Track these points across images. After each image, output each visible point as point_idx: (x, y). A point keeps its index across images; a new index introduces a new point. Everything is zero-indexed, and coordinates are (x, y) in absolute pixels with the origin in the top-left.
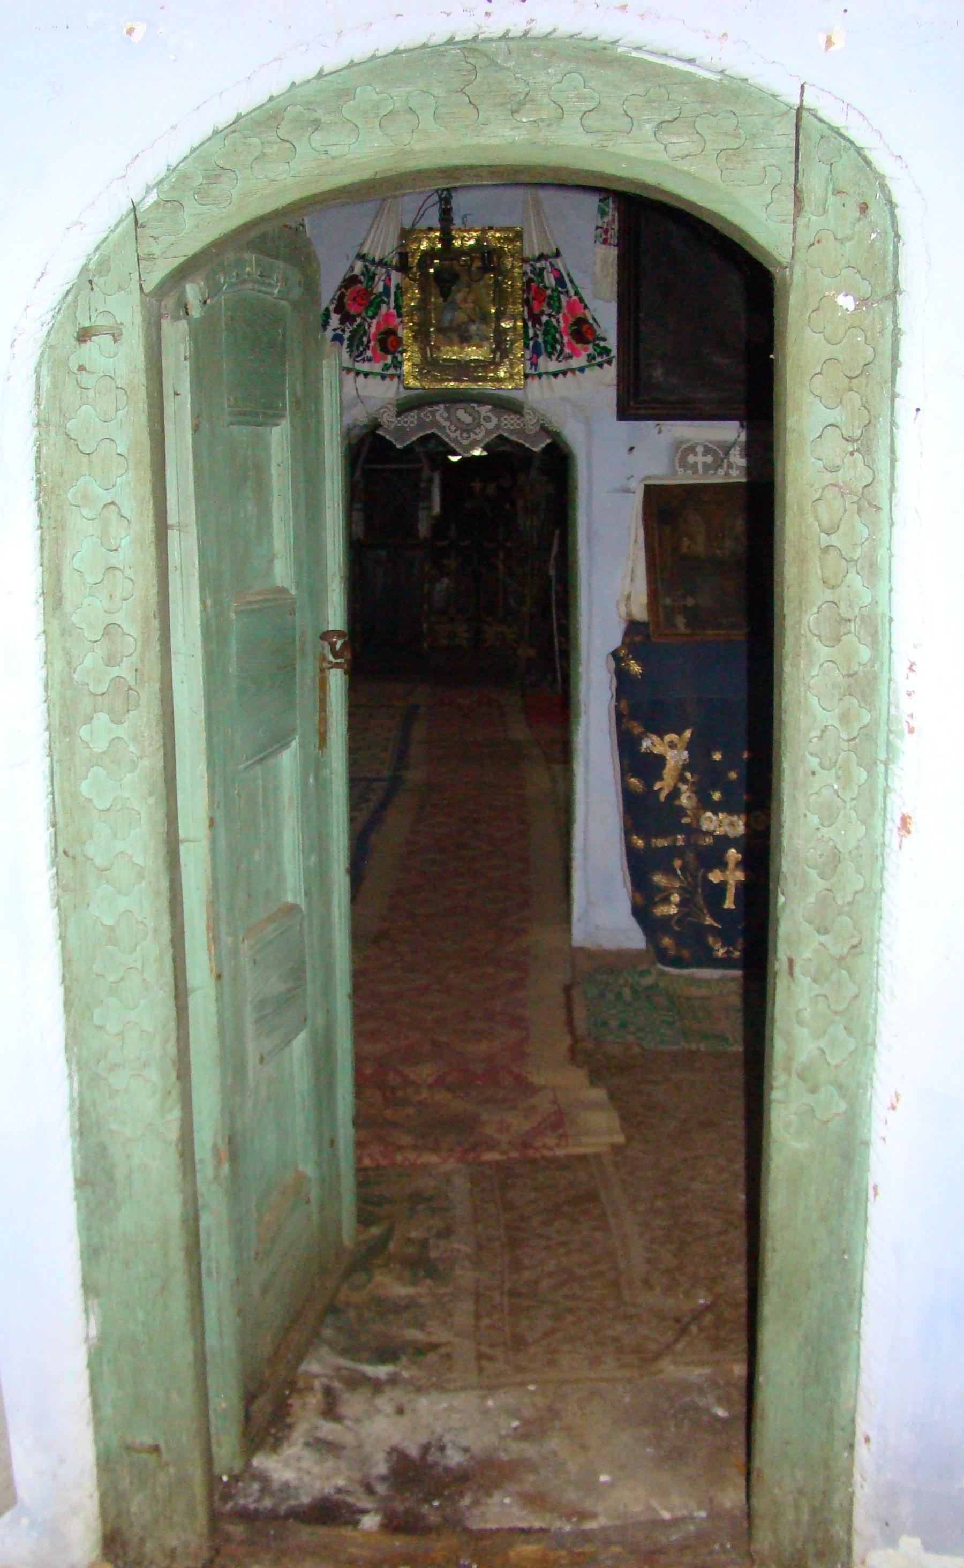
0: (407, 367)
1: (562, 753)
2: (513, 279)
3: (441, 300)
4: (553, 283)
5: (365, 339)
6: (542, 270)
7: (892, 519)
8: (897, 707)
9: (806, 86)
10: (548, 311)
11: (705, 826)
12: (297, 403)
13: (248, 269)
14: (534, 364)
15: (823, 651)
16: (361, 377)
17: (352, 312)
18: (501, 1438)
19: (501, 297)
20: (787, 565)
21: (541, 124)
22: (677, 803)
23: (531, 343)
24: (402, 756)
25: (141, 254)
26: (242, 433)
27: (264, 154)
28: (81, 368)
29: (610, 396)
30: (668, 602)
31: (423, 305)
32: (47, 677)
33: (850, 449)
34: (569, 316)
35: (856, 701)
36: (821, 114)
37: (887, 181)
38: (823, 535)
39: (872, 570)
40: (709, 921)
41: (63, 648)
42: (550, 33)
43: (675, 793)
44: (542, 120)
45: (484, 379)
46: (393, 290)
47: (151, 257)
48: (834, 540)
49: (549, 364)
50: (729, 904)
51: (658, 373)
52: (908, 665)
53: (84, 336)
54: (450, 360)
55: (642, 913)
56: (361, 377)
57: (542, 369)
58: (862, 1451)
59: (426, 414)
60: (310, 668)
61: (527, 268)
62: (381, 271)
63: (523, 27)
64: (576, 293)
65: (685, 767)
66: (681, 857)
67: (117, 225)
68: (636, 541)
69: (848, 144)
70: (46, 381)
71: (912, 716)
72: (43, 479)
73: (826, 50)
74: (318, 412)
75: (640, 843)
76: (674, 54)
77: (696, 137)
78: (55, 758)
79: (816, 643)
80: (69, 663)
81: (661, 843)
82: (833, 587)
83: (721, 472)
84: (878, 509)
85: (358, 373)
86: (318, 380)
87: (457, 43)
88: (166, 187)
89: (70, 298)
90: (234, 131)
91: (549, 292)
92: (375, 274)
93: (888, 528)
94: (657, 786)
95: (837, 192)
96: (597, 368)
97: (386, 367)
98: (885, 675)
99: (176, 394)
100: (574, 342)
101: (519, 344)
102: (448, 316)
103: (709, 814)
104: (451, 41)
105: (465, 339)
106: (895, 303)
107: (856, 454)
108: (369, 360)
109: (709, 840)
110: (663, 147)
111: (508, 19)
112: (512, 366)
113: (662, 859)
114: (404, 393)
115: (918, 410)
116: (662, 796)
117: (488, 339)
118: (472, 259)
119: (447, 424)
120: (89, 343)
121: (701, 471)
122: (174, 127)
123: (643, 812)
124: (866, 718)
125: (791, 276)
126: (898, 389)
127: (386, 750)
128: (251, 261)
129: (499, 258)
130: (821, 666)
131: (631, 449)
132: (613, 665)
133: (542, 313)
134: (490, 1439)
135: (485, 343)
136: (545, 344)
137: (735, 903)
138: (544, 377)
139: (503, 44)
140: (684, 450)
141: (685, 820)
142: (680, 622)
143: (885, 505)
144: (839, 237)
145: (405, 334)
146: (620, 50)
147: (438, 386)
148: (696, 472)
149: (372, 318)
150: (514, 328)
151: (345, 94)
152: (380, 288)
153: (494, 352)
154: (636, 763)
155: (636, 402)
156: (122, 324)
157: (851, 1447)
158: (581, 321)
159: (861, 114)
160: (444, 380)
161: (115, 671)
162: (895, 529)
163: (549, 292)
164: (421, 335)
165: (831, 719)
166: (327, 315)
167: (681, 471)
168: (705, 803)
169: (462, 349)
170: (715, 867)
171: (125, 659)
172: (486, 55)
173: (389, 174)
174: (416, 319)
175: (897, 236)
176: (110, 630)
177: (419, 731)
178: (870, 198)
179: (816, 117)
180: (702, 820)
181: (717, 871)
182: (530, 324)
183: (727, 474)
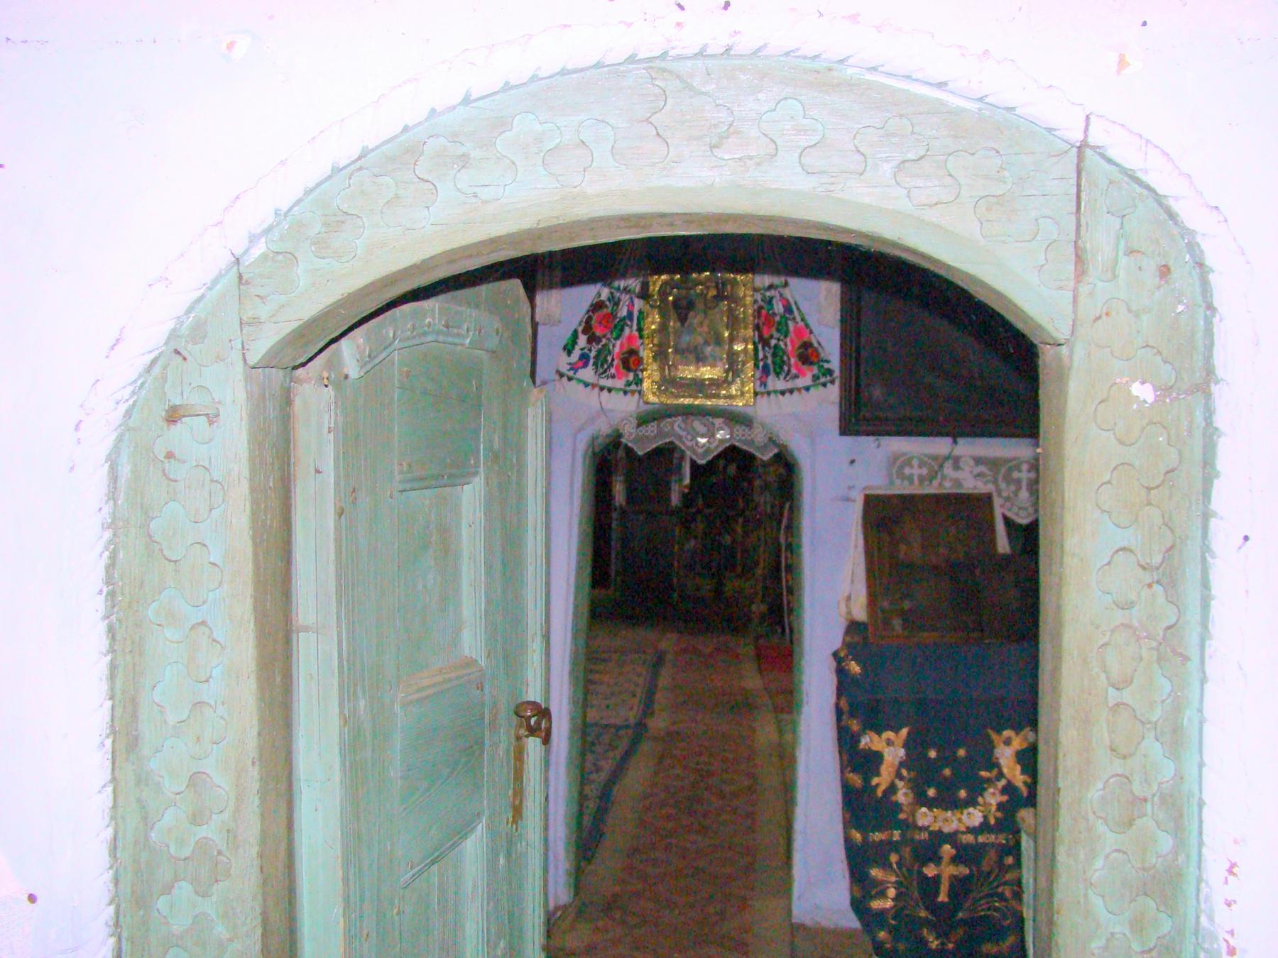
0: (646, 385)
1: (786, 701)
2: (744, 306)
3: (679, 324)
4: (781, 310)
5: (609, 358)
6: (771, 298)
7: (1204, 672)
8: (1211, 919)
9: (1092, 118)
10: (776, 335)
11: (921, 822)
12: (495, 457)
13: (427, 320)
14: (764, 384)
15: (1110, 839)
16: (605, 392)
17: (598, 333)
19: (733, 322)
21: (748, 162)
22: (894, 798)
23: (761, 364)
25: (244, 318)
26: (423, 498)
27: (397, 197)
28: (170, 455)
29: (833, 412)
30: (885, 604)
31: (663, 328)
32: (115, 838)
33: (1149, 581)
34: (796, 340)
35: (1152, 904)
36: (1111, 153)
37: (1199, 239)
38: (1111, 690)
39: (1177, 735)
40: (923, 914)
41: (139, 801)
42: (759, 50)
43: (892, 789)
44: (751, 158)
45: (718, 396)
46: (636, 314)
47: (255, 322)
48: (1126, 696)
49: (775, 383)
50: (943, 897)
51: (877, 392)
52: (1227, 865)
53: (173, 416)
54: (685, 378)
55: (859, 906)
56: (605, 392)
57: (770, 387)
59: (666, 424)
60: (503, 737)
61: (758, 297)
62: (625, 298)
63: (725, 41)
64: (803, 320)
65: (902, 764)
66: (897, 851)
67: (215, 282)
68: (856, 547)
69: (1145, 192)
70: (125, 471)
71: (1232, 933)
72: (118, 591)
73: (1119, 72)
74: (521, 467)
75: (858, 836)
76: (919, 76)
77: (948, 180)
78: (125, 934)
79: (1100, 827)
80: (145, 818)
81: (877, 836)
82: (1125, 757)
83: (935, 483)
84: (1186, 659)
85: (602, 389)
86: (522, 427)
87: (640, 61)
88: (276, 234)
89: (157, 370)
90: (361, 169)
91: (777, 319)
92: (619, 300)
93: (1197, 684)
94: (875, 781)
95: (1131, 252)
96: (821, 388)
97: (629, 384)
98: (1192, 868)
99: (318, 471)
100: (800, 364)
101: (750, 365)
102: (686, 339)
103: (924, 809)
104: (632, 59)
105: (700, 359)
106: (1208, 395)
107: (1155, 586)
108: (613, 377)
109: (924, 836)
110: (905, 192)
111: (705, 30)
112: (743, 384)
113: (878, 854)
114: (643, 408)
115: (1246, 538)
116: (879, 793)
117: (721, 359)
118: (708, 288)
119: (684, 434)
120: (179, 424)
121: (916, 482)
122: (283, 163)
123: (861, 806)
124: (1166, 926)
125: (1071, 356)
126: (1215, 505)
127: (634, 696)
128: (433, 311)
129: (732, 287)
130: (1107, 857)
131: (852, 462)
132: (835, 664)
133: (772, 337)
135: (719, 364)
136: (772, 365)
137: (949, 896)
138: (772, 396)
139: (699, 63)
140: (898, 464)
141: (902, 816)
142: (897, 623)
143: (1194, 653)
144: (1134, 308)
145: (646, 354)
146: (850, 71)
147: (675, 402)
148: (912, 482)
149: (616, 339)
150: (745, 350)
151: (501, 124)
152: (623, 312)
153: (727, 371)
154: (857, 761)
155: (858, 418)
156: (219, 402)
158: (807, 345)
159: (1165, 154)
160: (677, 397)
161: (202, 832)
162: (1208, 687)
163: (777, 319)
164: (660, 355)
165: (1119, 927)
166: (575, 335)
167: (898, 482)
168: (921, 800)
169: (698, 369)
170: (930, 860)
171: (214, 816)
172: (678, 77)
173: (555, 222)
174: (656, 341)
175: (1210, 307)
176: (196, 781)
178: (1176, 261)
179: (1103, 156)
180: (918, 815)
181: (932, 865)
182: (760, 347)
183: (940, 485)
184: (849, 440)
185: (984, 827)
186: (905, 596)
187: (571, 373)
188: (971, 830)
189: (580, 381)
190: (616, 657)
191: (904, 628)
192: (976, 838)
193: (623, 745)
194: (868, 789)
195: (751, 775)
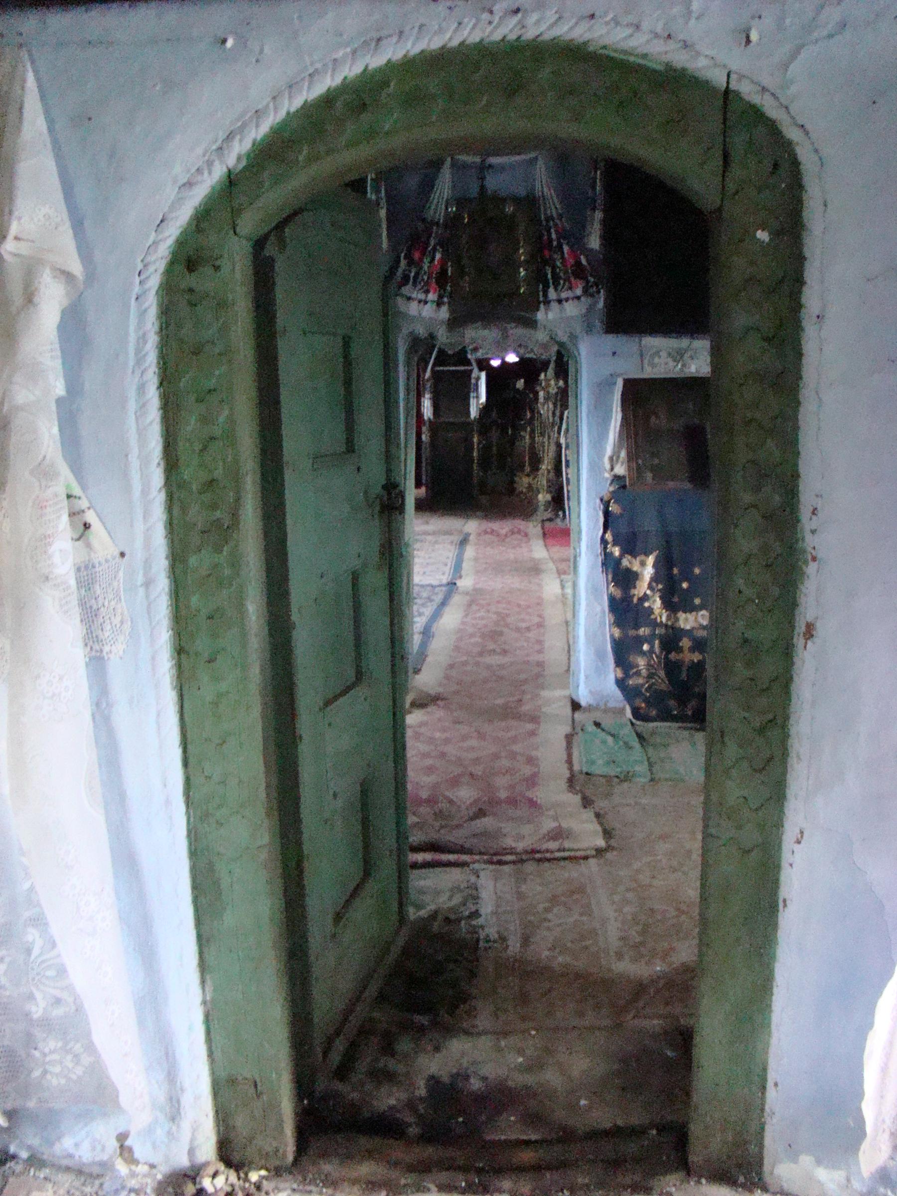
18: (510, 1070)
20: (167, 590)
24: (458, 568)
50: (684, 676)
52: (811, 509)
58: (771, 1094)
71: (814, 548)
116: (635, 600)
127: (446, 565)
131: (614, 353)
134: (502, 1072)
142: (649, 476)
157: (764, 1088)
177: (470, 552)
184: (610, 337)
186: (653, 455)
190: (429, 538)
193: (438, 598)
194: (627, 598)
195: (540, 616)
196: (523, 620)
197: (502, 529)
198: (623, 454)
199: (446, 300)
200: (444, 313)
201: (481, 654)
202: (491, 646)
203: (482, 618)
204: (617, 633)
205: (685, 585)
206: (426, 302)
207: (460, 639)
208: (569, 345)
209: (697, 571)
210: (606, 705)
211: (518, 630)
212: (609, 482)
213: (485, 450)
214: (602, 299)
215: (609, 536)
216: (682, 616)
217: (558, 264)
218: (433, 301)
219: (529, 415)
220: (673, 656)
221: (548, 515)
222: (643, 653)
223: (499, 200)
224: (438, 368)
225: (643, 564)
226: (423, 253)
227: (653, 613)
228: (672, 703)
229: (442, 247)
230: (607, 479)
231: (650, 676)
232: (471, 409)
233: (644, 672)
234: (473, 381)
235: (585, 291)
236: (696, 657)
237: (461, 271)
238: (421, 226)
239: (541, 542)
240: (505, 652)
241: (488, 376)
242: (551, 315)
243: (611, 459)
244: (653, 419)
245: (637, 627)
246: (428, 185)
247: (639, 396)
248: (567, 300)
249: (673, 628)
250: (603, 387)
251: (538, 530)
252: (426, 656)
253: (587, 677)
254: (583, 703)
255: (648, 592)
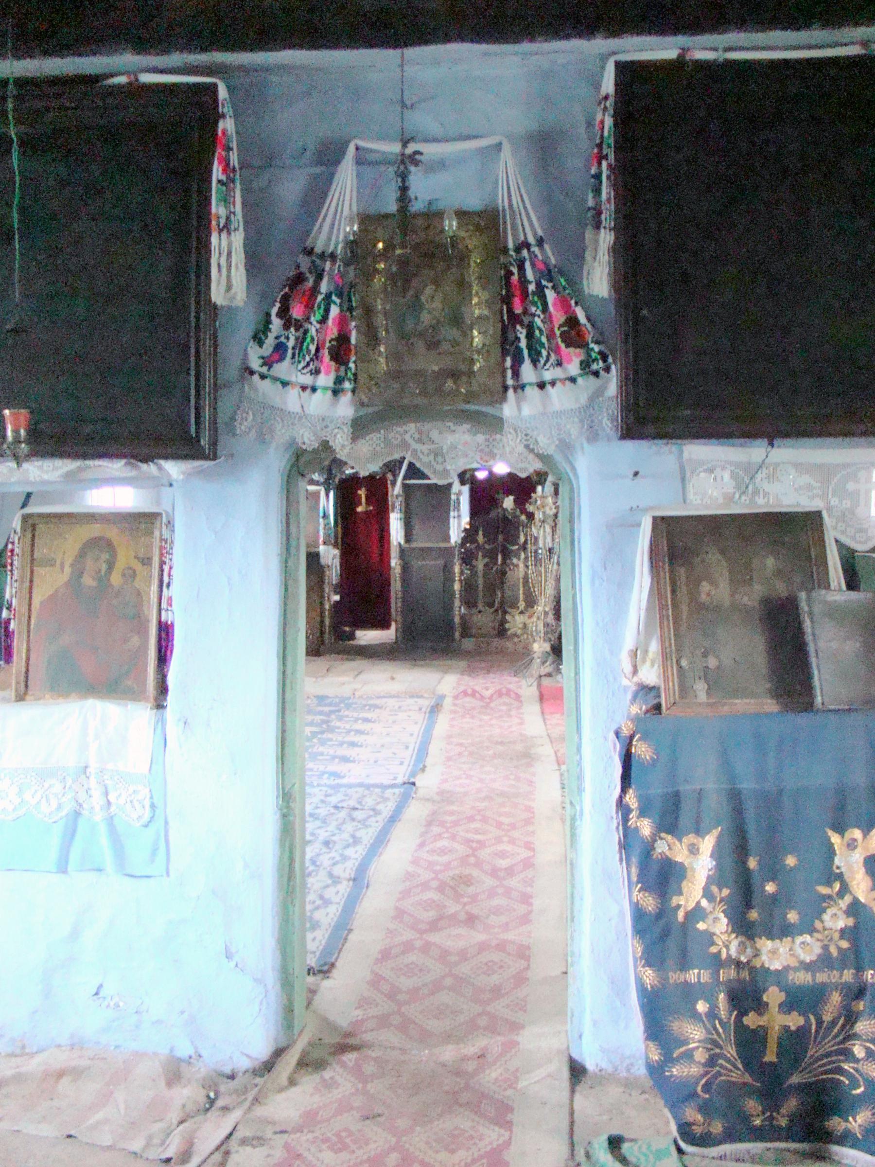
116: (681, 915)
131: (636, 474)
142: (700, 687)
184: (630, 446)
185: (825, 961)
187: (264, 369)
188: (807, 967)
189: (276, 379)
190: (392, 703)
191: (708, 693)
192: (814, 976)
193: (387, 809)
194: (664, 912)
195: (529, 846)
196: (503, 855)
197: (487, 689)
198: (654, 647)
199: (347, 385)
200: (345, 408)
201: (434, 926)
202: (453, 908)
203: (443, 851)
204: (649, 976)
205: (770, 888)
206: (314, 389)
207: (406, 894)
208: (558, 458)
209: (791, 861)
210: (628, 1070)
211: (494, 872)
212: (629, 696)
213: (469, 587)
214: (615, 380)
215: (631, 799)
216: (766, 945)
217: (538, 321)
218: (325, 388)
219: (522, 539)
220: (751, 1020)
221: (548, 668)
222: (695, 1016)
223: (433, 216)
224: (408, 482)
225: (694, 850)
226: (309, 306)
227: (713, 943)
228: (752, 1105)
229: (340, 295)
230: (626, 689)
231: (712, 1061)
232: (451, 533)
233: (700, 1056)
234: (453, 497)
235: (585, 365)
236: (794, 1021)
237: (372, 337)
238: (305, 262)
239: (537, 708)
240: (471, 920)
241: (472, 491)
242: (527, 410)
243: (634, 654)
244: (705, 586)
245: (684, 965)
246: (316, 196)
247: (679, 544)
248: (553, 383)
249: (752, 970)
250: (620, 527)
251: (534, 691)
252: (350, 931)
253: (595, 1023)
254: (590, 1065)
255: (704, 903)
